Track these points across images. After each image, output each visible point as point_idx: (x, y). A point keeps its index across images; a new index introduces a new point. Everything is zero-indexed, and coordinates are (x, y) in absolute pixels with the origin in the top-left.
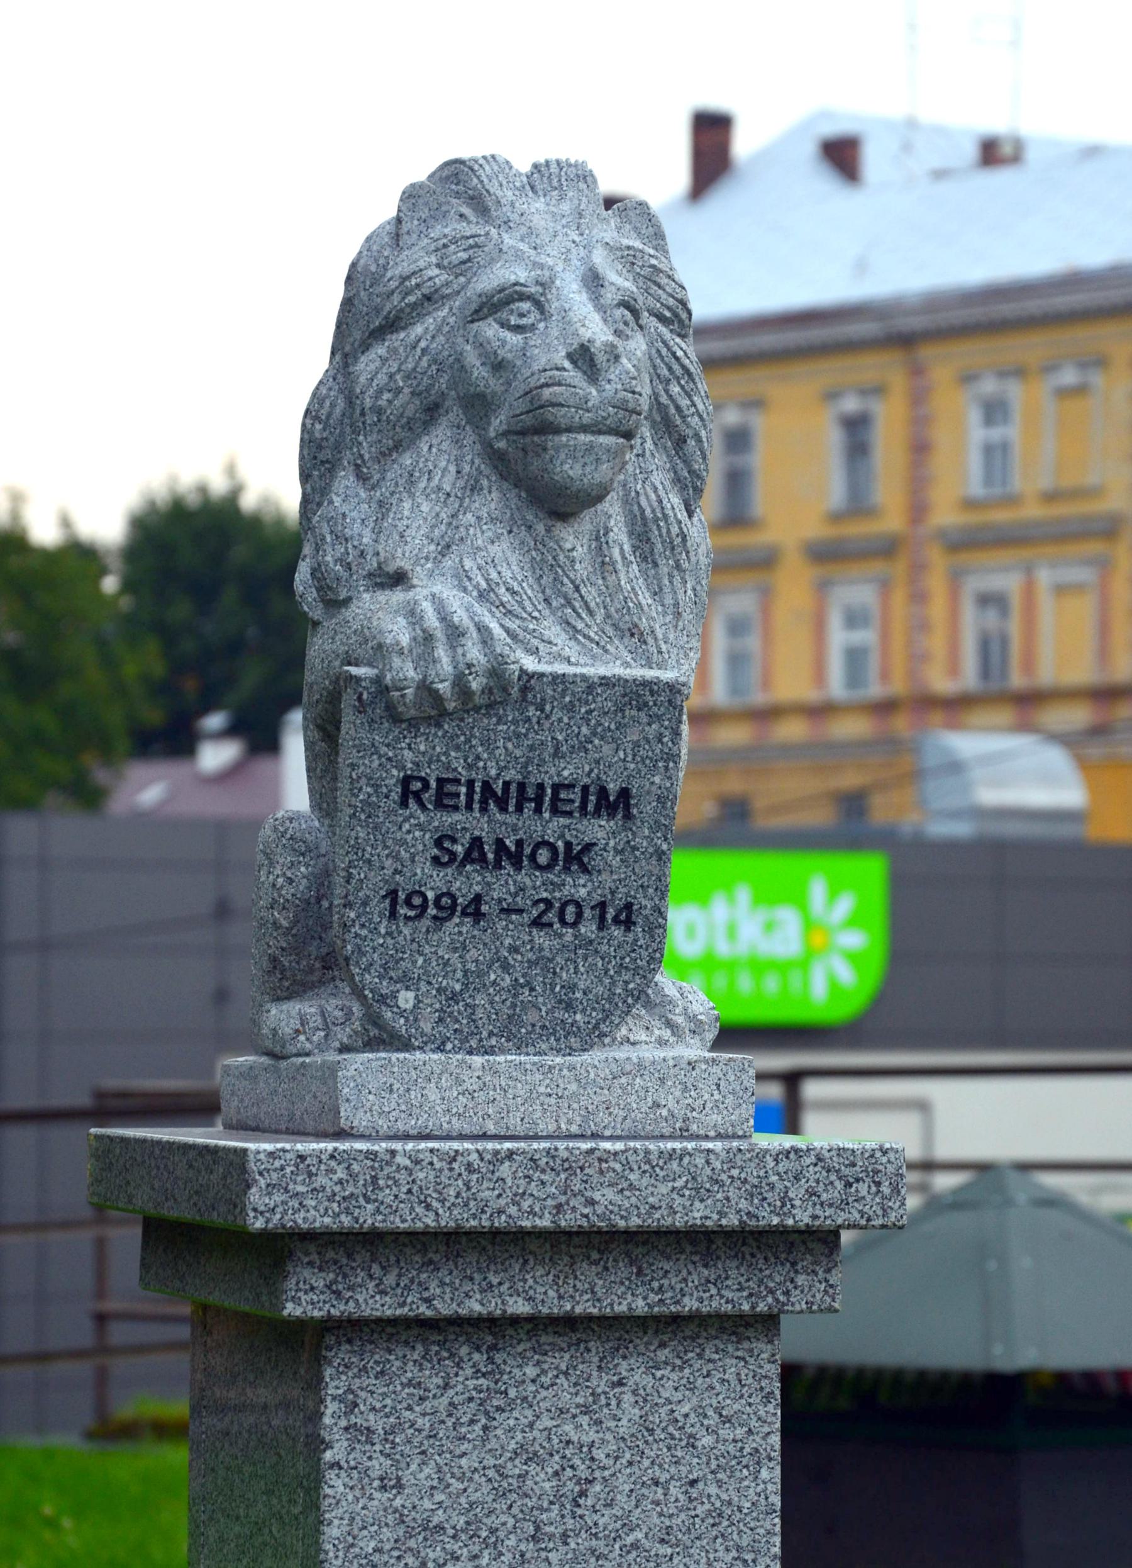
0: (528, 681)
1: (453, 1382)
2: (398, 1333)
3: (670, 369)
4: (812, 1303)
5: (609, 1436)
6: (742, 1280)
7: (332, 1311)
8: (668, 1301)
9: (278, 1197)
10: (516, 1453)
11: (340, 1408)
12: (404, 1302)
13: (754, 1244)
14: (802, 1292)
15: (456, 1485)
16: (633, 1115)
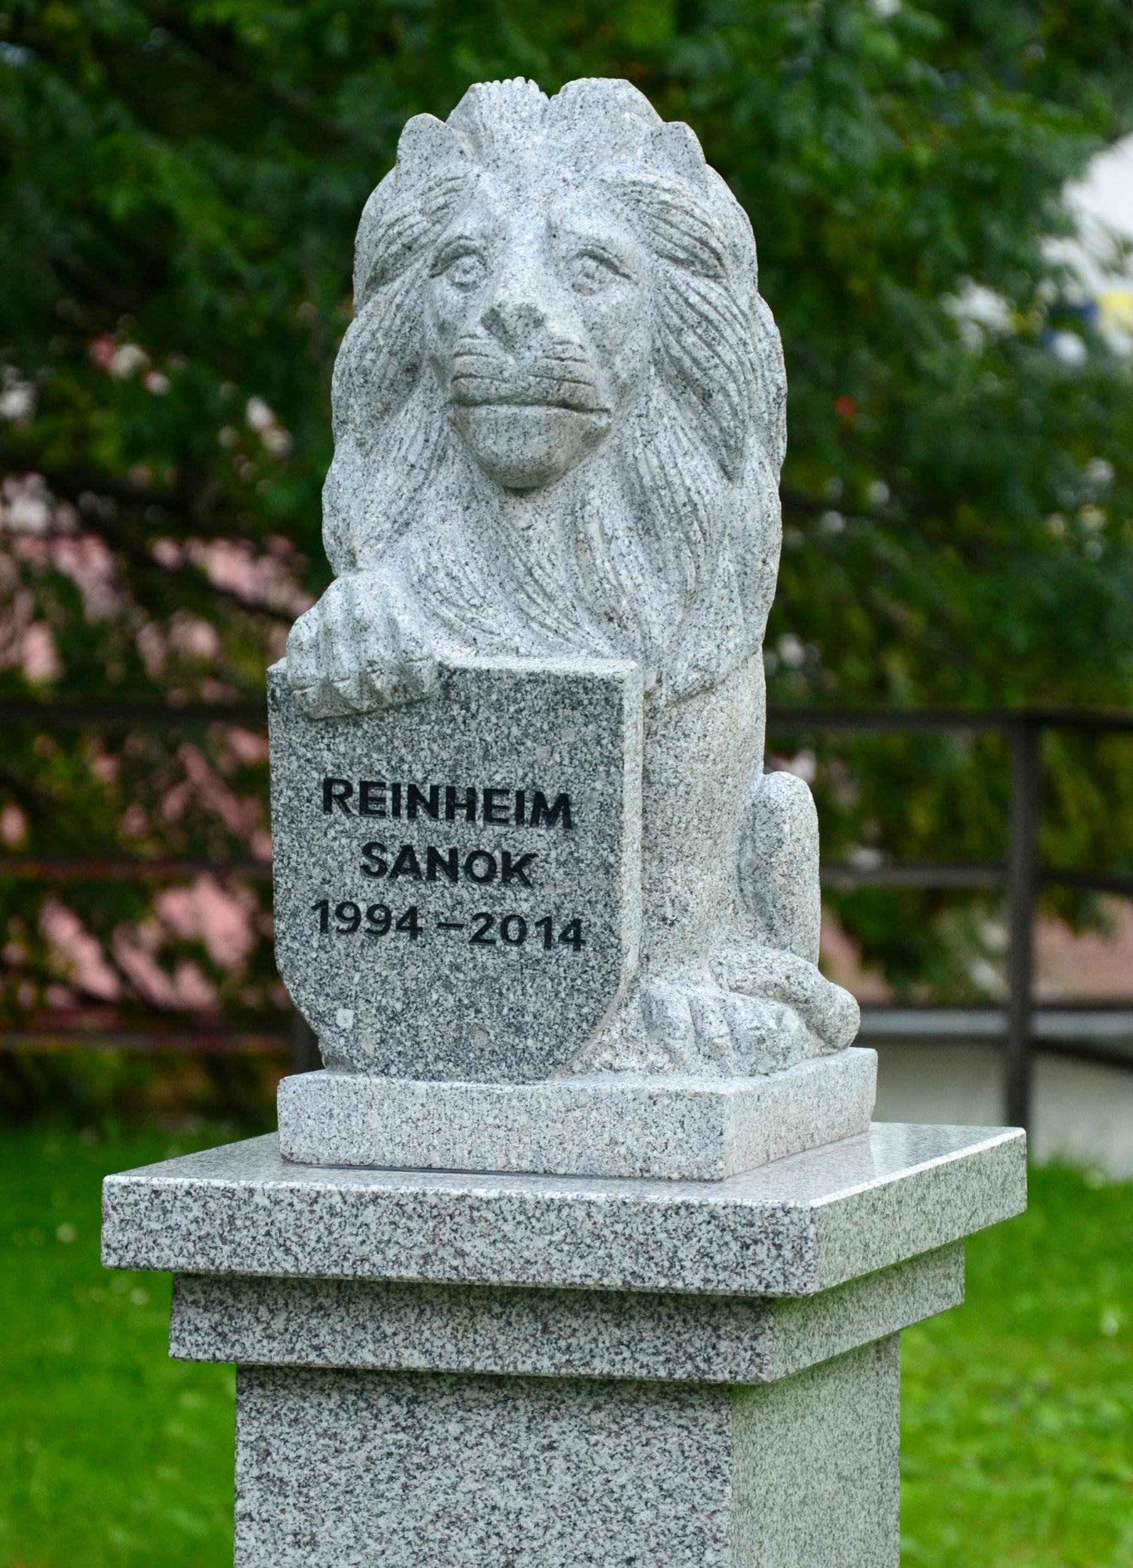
0: (450, 677)
1: (370, 1435)
2: (313, 1378)
3: (682, 317)
4: (737, 1373)
5: (538, 1504)
6: (658, 1343)
7: (218, 1354)
8: (576, 1363)
10: (437, 1515)
11: (252, 1456)
12: (293, 1349)
13: (672, 1305)
14: (725, 1360)
15: (374, 1547)
16: (588, 1152)
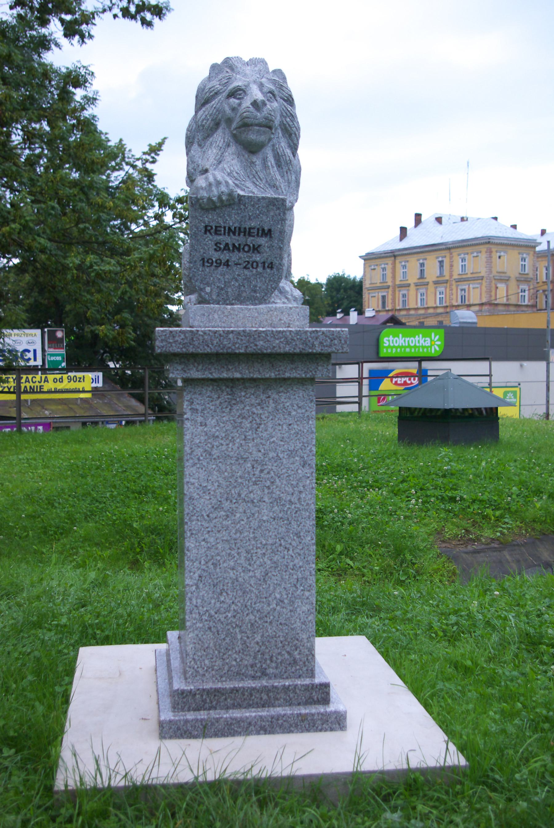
9: (164, 343)
15: (222, 425)
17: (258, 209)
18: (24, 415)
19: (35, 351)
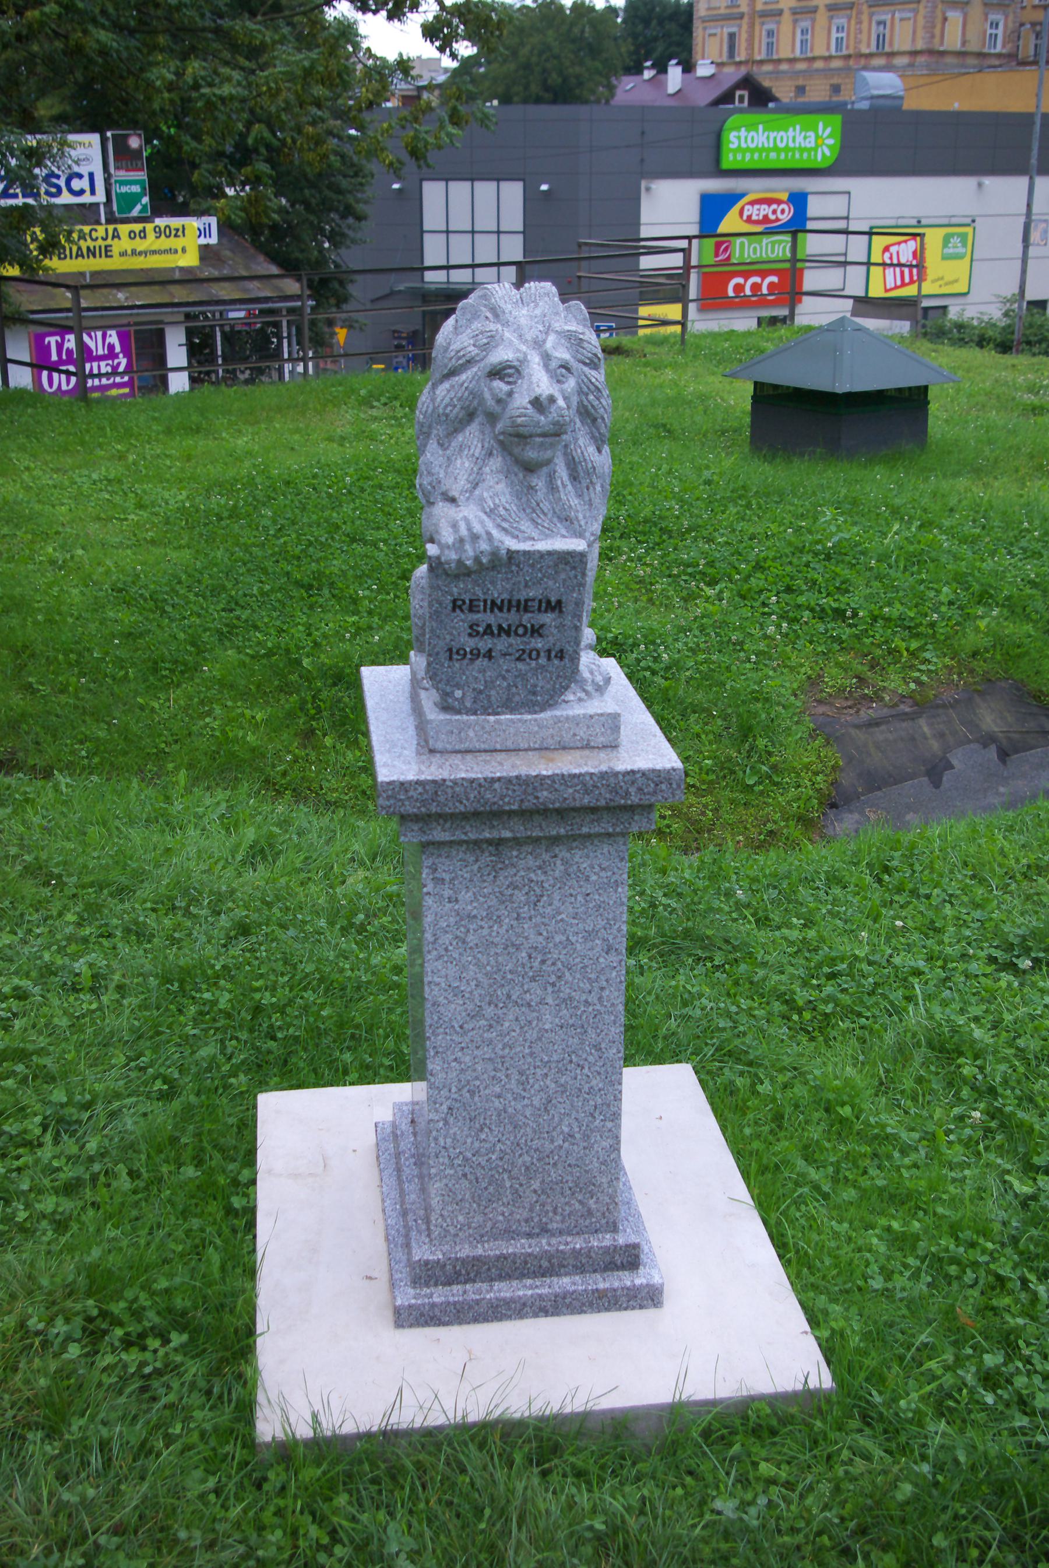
9: (392, 801)
17: (540, 570)
18: (84, 304)
19: (91, 176)
